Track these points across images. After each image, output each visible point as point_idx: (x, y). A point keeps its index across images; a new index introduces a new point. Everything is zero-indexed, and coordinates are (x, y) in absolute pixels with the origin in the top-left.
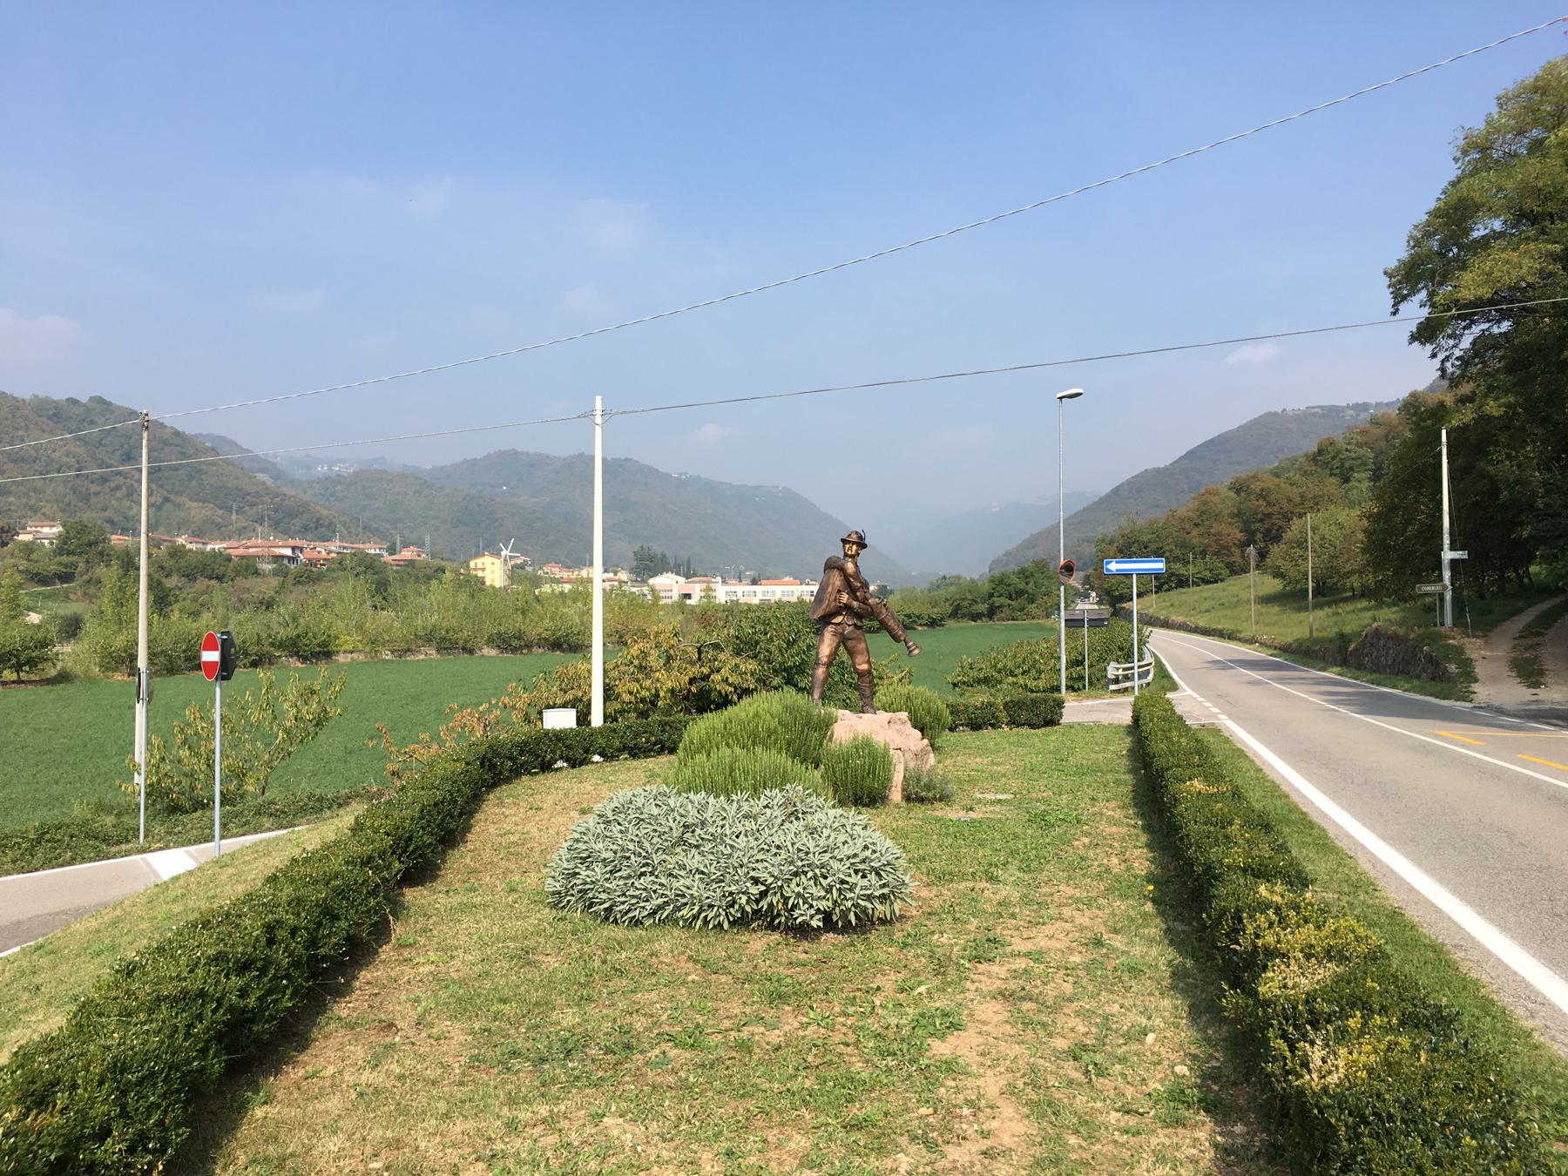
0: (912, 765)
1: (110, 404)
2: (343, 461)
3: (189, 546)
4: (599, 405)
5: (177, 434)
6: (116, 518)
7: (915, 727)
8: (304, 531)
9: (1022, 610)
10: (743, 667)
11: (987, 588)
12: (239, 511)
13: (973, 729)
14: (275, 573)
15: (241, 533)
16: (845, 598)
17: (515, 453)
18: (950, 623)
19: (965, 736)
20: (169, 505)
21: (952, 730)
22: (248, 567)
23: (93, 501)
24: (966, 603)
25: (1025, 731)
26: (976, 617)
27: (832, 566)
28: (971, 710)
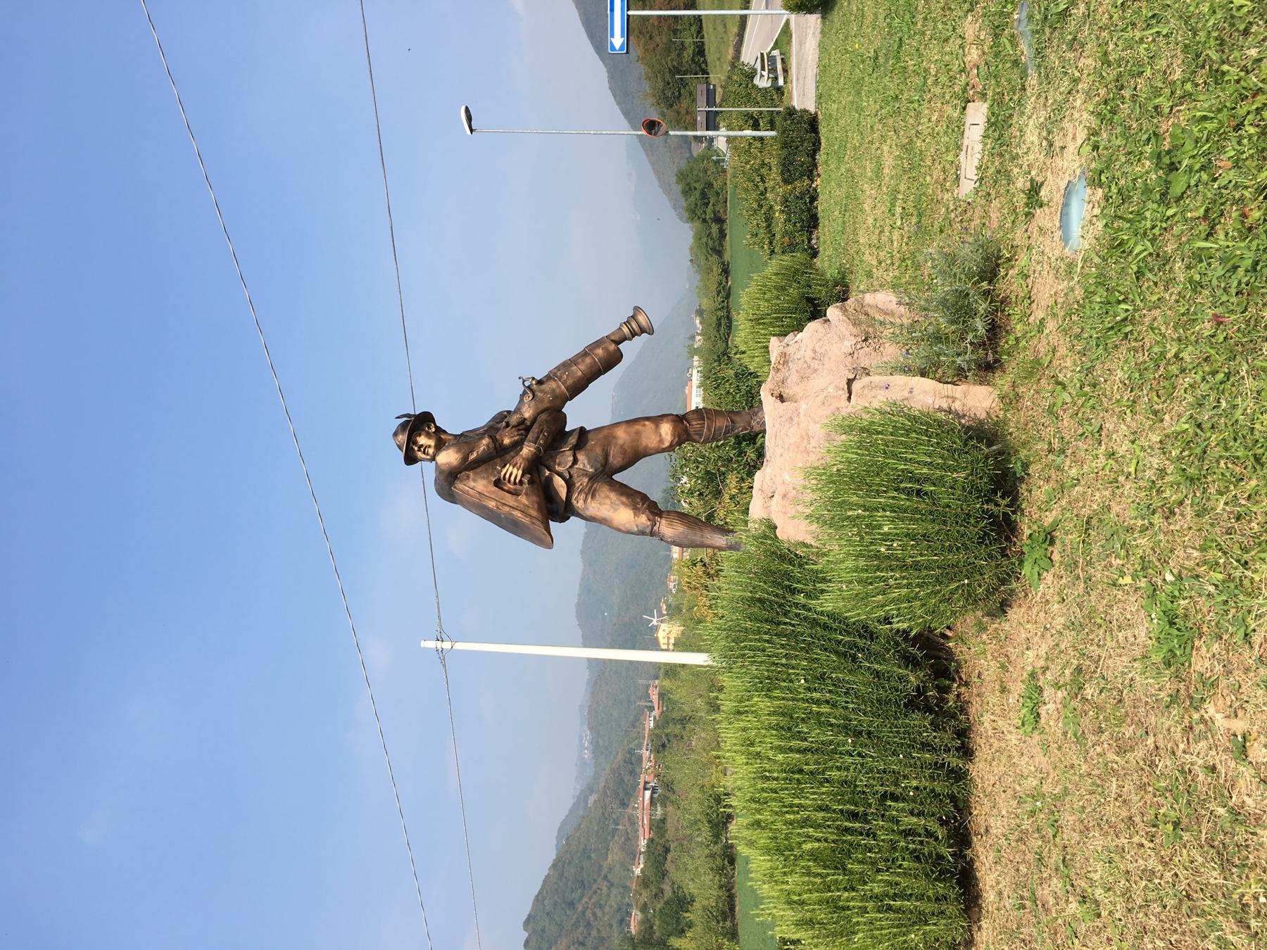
0: (891, 352)
1: (529, 915)
2: (581, 739)
3: (642, 866)
4: (431, 644)
5: (554, 866)
6: (618, 917)
7: (800, 328)
8: (634, 774)
9: (718, 194)
10: (734, 491)
11: (698, 224)
12: (616, 823)
13: (816, 226)
14: (664, 806)
15: (633, 822)
16: (513, 471)
17: (578, 605)
18: (727, 257)
19: (825, 235)
20: (609, 876)
21: (815, 254)
22: (658, 827)
23: (604, 934)
24: (710, 243)
25: (821, 157)
26: (722, 235)
27: (448, 483)
28: (790, 227)
